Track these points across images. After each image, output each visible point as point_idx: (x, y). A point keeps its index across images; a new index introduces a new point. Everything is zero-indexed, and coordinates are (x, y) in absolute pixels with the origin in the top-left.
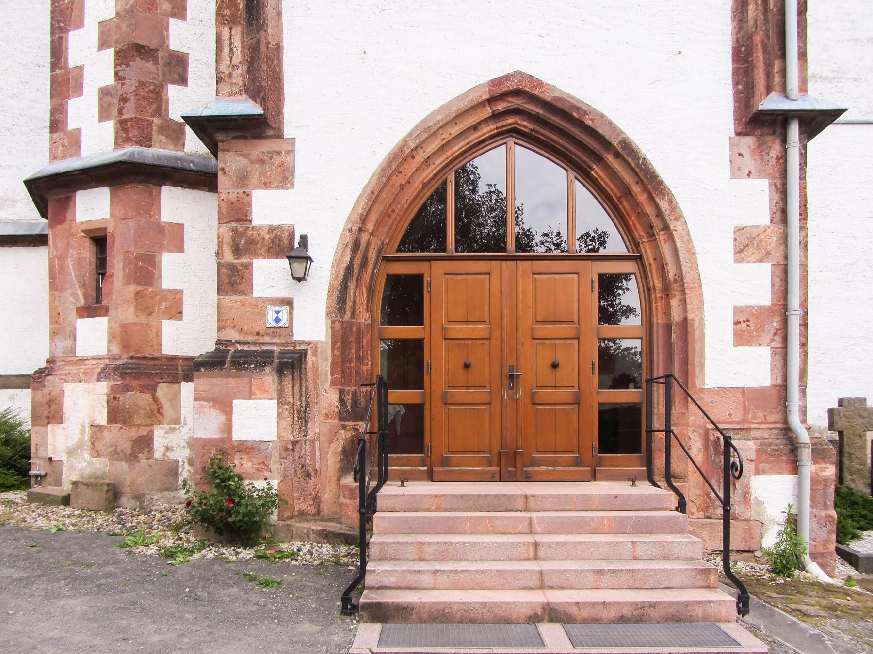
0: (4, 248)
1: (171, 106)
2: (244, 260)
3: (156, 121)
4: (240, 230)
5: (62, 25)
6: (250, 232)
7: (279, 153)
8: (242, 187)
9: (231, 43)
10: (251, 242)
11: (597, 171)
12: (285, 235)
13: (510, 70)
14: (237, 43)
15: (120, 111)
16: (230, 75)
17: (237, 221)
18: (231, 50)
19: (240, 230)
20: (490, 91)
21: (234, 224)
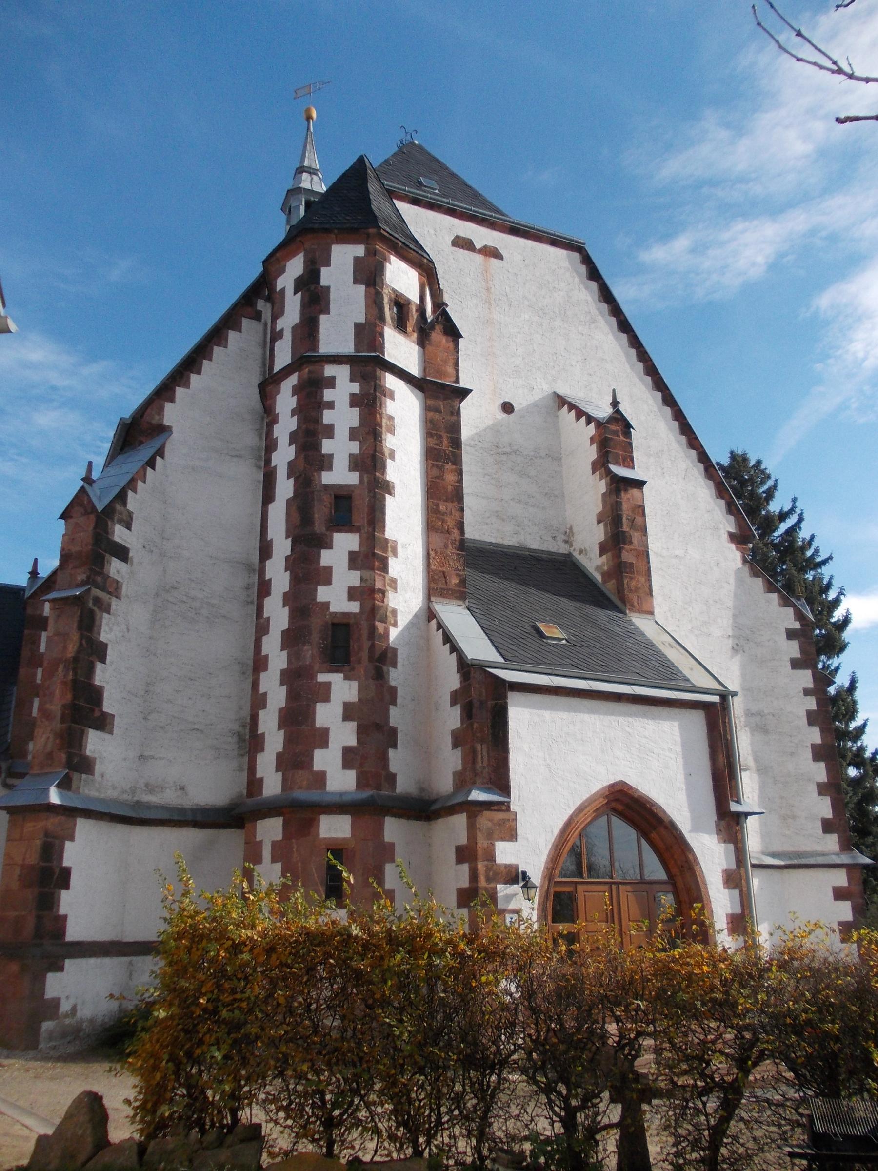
0: (150, 827)
1: (390, 763)
2: (492, 885)
3: (384, 773)
4: (490, 866)
5: (310, 696)
6: (494, 867)
7: (508, 820)
8: (489, 839)
9: (482, 754)
10: (496, 874)
11: (653, 835)
12: (513, 870)
13: (618, 779)
14: (485, 753)
15: (361, 765)
16: (482, 772)
17: (488, 860)
18: (482, 757)
19: (490, 866)
20: (609, 791)
21: (486, 863)
